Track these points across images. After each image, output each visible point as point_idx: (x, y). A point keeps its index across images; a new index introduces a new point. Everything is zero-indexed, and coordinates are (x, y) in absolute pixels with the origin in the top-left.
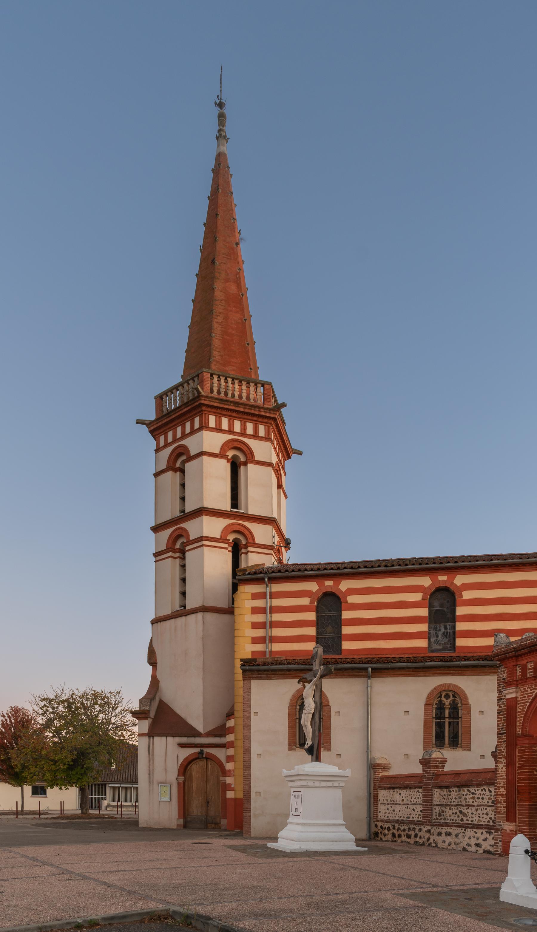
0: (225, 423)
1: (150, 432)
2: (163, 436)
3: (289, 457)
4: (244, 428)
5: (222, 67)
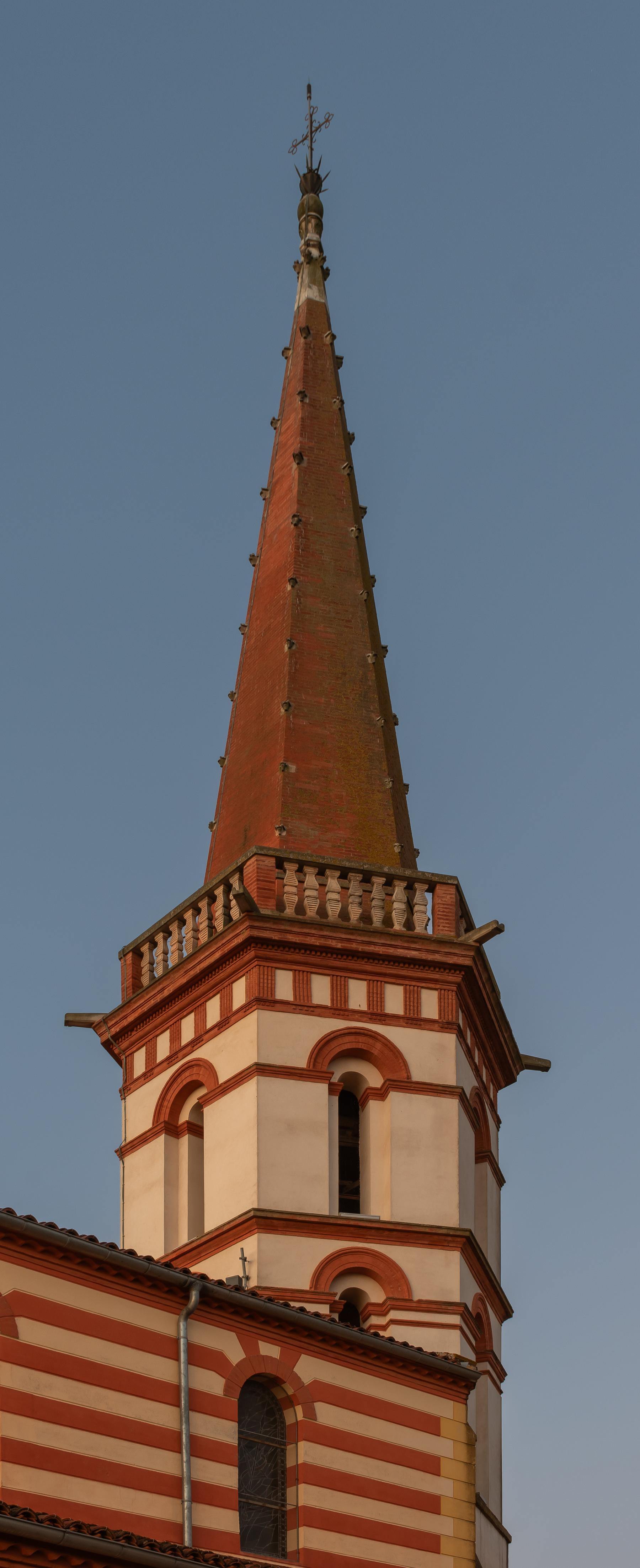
0: (321, 989)
1: (107, 1045)
2: (167, 1034)
3: (510, 1079)
4: (376, 997)
5: (309, 87)
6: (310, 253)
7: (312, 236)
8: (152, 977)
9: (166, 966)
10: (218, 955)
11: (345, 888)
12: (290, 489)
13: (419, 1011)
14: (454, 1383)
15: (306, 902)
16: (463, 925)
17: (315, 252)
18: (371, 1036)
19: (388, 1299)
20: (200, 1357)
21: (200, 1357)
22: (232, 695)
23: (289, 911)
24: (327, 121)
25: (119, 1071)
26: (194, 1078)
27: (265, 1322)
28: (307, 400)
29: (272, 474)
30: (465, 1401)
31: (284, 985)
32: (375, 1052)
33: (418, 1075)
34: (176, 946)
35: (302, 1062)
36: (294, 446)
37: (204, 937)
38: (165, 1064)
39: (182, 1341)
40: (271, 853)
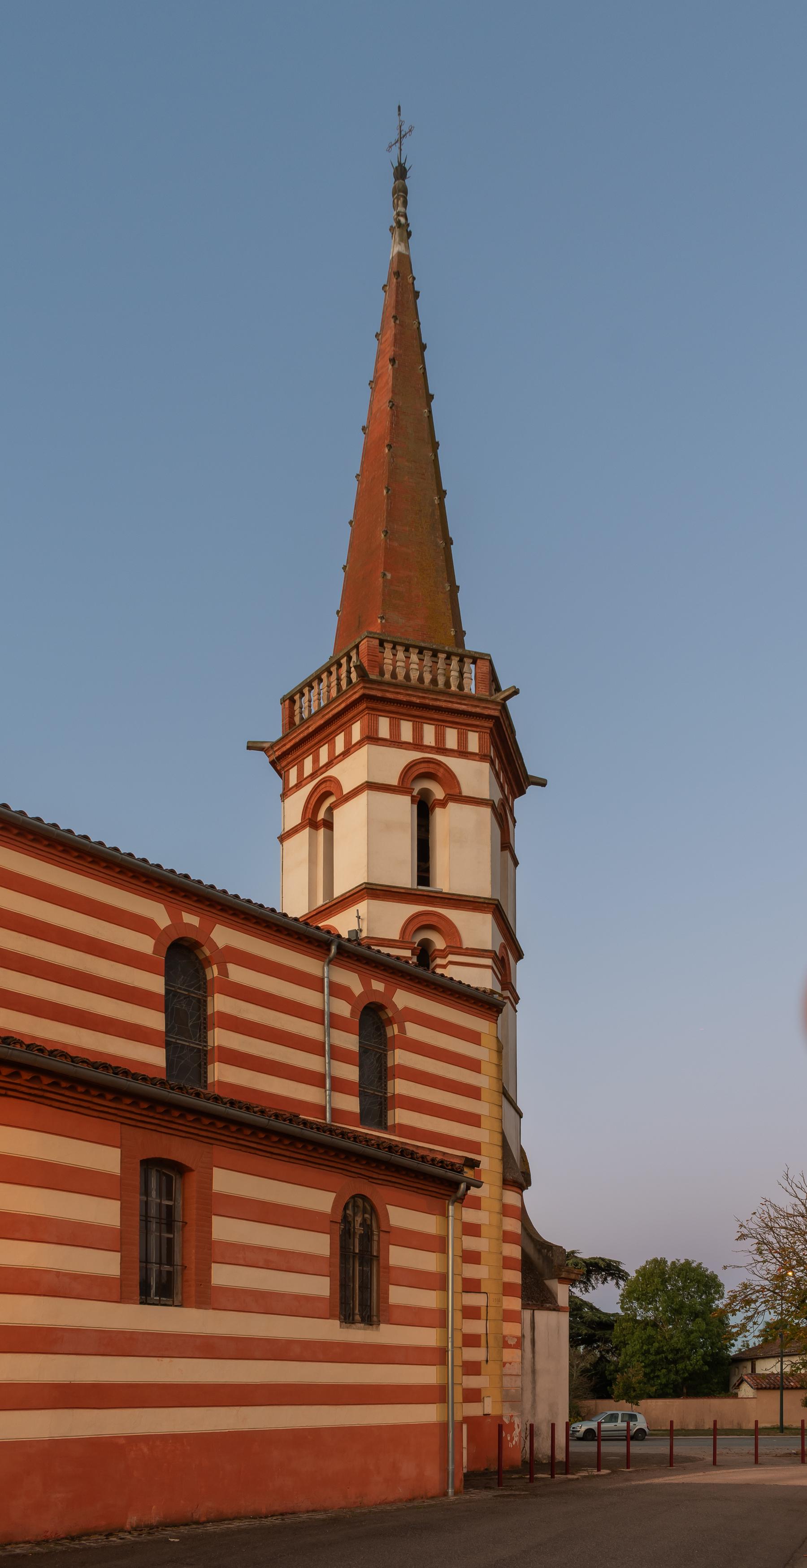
0: (406, 731)
1: (273, 763)
2: (311, 757)
3: (522, 792)
4: (440, 737)
5: (399, 107)
6: (399, 221)
7: (401, 209)
8: (302, 718)
9: (310, 711)
10: (343, 705)
11: (421, 660)
12: (387, 382)
13: (466, 747)
14: (489, 1009)
15: (397, 670)
16: (494, 686)
17: (403, 220)
18: (437, 764)
19: (448, 946)
20: (337, 991)
21: (337, 991)
22: (351, 523)
23: (387, 676)
24: (410, 131)
25: (281, 781)
26: (328, 789)
27: (376, 967)
28: (398, 322)
29: (376, 371)
30: (496, 1021)
31: (384, 727)
32: (440, 775)
33: (466, 791)
34: (316, 697)
35: (395, 782)
36: (390, 354)
37: (334, 693)
38: (309, 779)
39: (326, 980)
40: (376, 636)
